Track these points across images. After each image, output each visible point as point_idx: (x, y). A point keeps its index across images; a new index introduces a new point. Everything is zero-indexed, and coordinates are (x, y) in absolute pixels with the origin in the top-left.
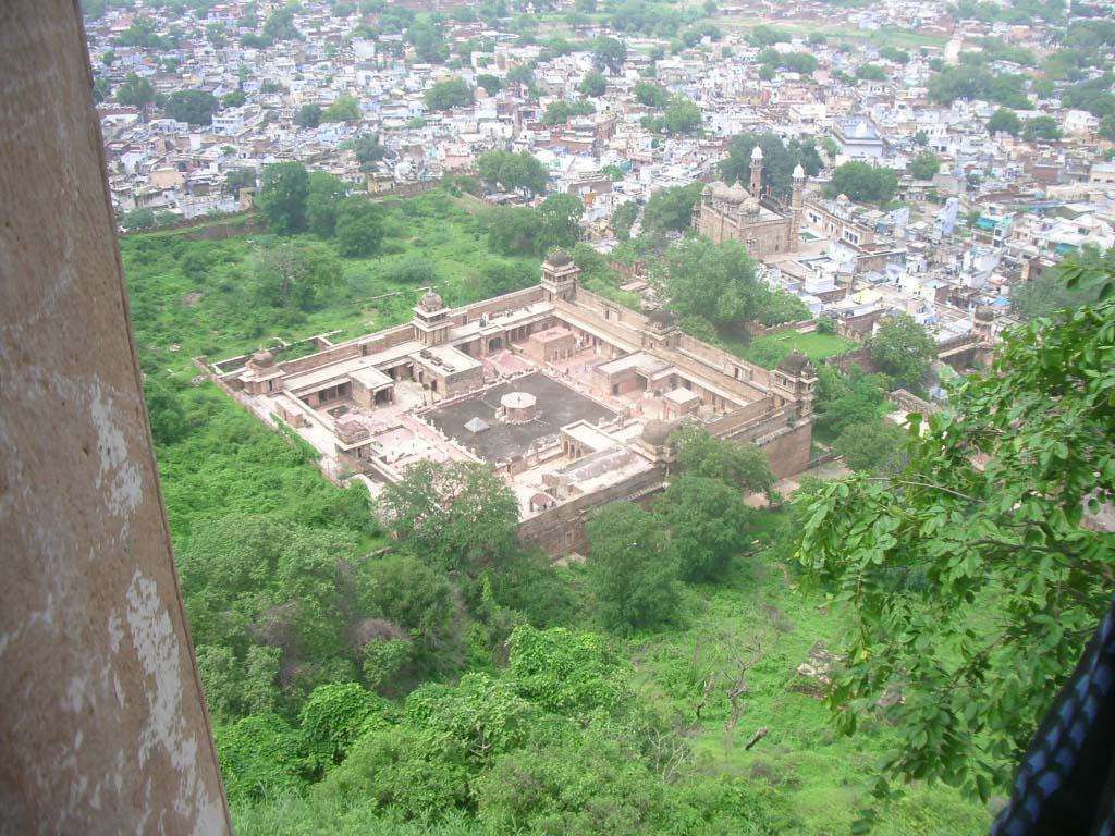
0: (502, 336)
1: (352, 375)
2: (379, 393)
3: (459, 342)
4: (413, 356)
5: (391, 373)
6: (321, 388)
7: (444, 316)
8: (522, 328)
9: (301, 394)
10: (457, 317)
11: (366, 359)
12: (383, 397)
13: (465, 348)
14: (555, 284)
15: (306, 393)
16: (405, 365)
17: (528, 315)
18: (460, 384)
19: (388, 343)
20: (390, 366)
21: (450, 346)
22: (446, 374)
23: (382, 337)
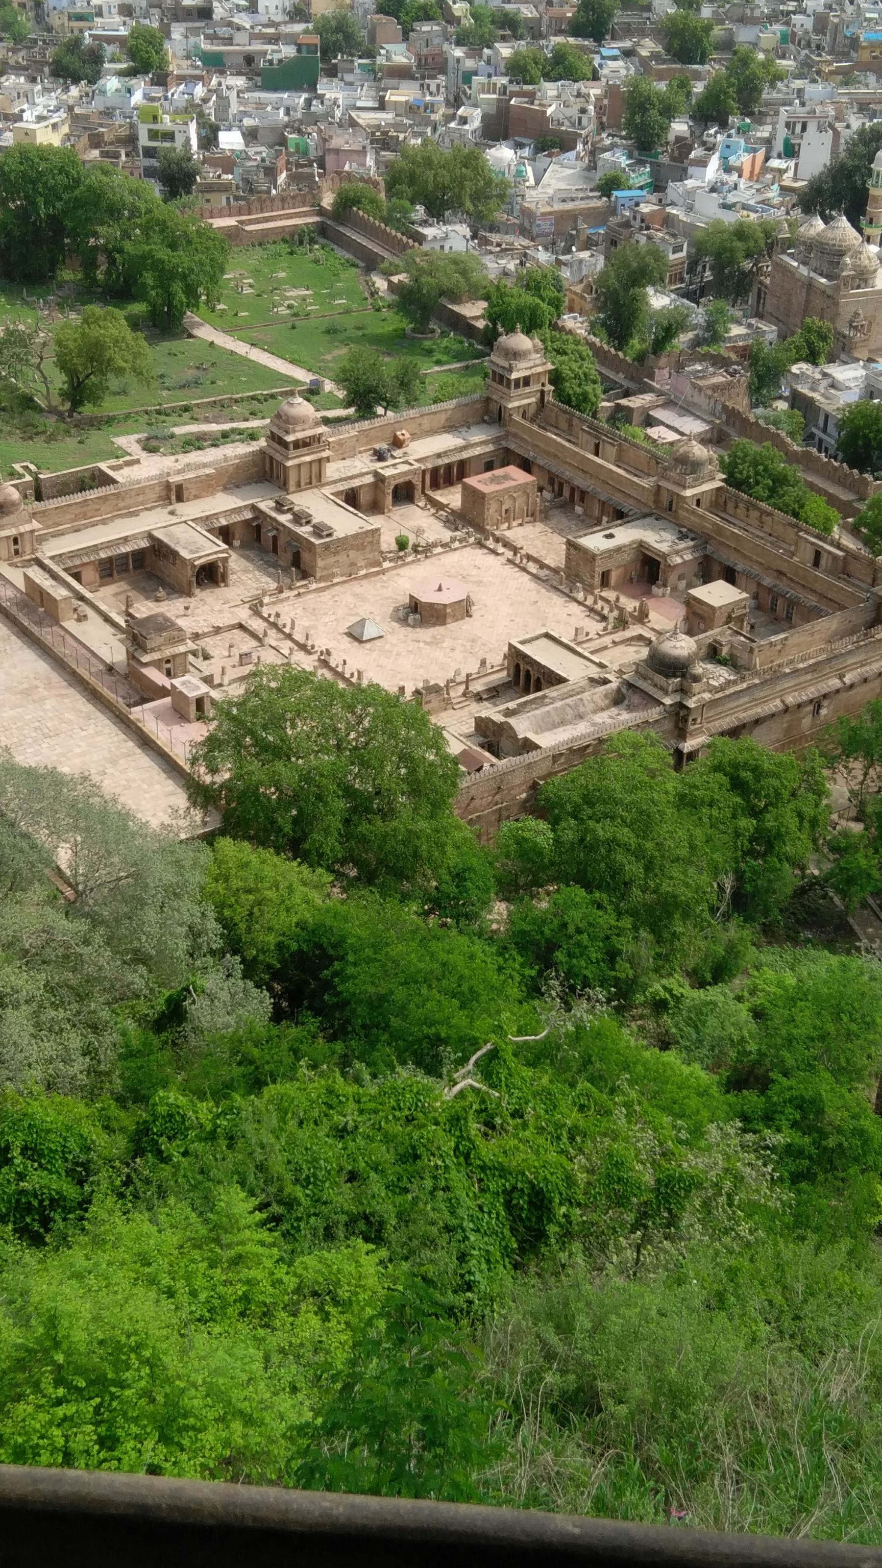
0: (417, 481)
2: (203, 568)
3: (341, 487)
5: (225, 534)
7: (317, 439)
8: (449, 467)
11: (179, 507)
13: (351, 498)
15: (77, 562)
16: (247, 523)
18: (342, 558)
20: (224, 522)
21: (327, 491)
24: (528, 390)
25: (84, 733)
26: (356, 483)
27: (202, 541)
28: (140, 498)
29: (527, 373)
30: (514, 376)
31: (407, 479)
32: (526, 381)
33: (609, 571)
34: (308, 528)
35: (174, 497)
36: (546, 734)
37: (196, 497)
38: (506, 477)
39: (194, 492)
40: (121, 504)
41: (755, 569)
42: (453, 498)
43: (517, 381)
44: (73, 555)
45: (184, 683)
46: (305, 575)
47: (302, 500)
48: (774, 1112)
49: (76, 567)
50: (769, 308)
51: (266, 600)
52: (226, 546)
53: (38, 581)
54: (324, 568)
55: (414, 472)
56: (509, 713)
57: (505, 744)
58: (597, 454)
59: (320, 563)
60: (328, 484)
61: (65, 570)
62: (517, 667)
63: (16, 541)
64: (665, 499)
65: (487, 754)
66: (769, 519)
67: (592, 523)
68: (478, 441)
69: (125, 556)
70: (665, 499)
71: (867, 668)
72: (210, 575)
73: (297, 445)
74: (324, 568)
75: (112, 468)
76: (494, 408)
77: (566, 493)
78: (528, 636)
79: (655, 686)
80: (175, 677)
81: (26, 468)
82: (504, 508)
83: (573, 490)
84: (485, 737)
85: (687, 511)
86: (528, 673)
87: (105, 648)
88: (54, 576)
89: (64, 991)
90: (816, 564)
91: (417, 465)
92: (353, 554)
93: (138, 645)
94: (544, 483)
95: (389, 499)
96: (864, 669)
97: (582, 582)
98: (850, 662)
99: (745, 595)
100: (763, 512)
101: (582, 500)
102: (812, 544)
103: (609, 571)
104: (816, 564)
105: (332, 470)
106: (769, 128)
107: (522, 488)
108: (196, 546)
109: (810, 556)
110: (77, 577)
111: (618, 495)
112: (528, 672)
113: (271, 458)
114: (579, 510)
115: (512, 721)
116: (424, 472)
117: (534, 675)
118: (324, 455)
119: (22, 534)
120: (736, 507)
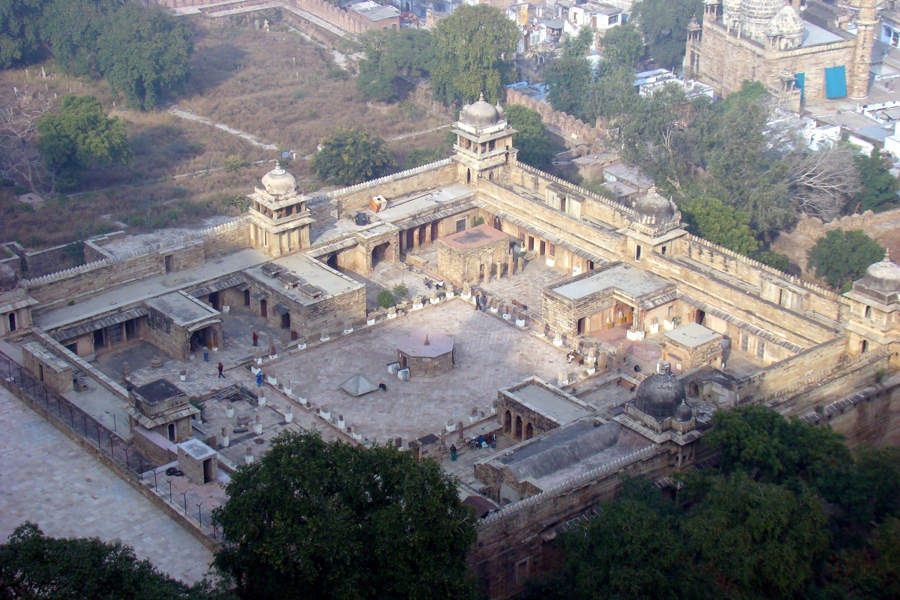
2: (196, 334)
4: (250, 272)
5: (214, 299)
11: (173, 277)
12: (200, 339)
14: (478, 155)
22: (307, 302)
25: (96, 502)
28: (132, 271)
36: (545, 478)
39: (183, 263)
40: (114, 277)
41: (725, 310)
44: (70, 328)
45: (191, 447)
48: (536, 317)
49: (72, 339)
50: (703, 68)
53: (37, 355)
56: (507, 460)
61: (62, 342)
62: (508, 412)
63: (12, 317)
66: (733, 262)
78: (516, 384)
79: (645, 425)
80: (181, 440)
81: (13, 247)
83: (543, 245)
84: (485, 483)
86: (518, 418)
87: (107, 417)
88: (53, 351)
93: (142, 411)
100: (726, 257)
101: (553, 253)
110: (73, 348)
111: (459, 210)
113: (256, 226)
115: (512, 466)
119: (18, 310)
120: (701, 253)
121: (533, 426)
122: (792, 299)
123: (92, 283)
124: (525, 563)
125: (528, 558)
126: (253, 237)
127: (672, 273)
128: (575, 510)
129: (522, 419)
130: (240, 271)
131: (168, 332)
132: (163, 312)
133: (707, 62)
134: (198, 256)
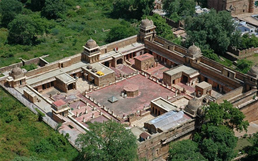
1: (57, 77)
2: (69, 85)
3: (104, 61)
5: (74, 75)
6: (43, 83)
7: (97, 50)
9: (34, 86)
10: (102, 50)
13: (106, 64)
15: (36, 85)
17: (133, 48)
19: (69, 63)
21: (100, 62)
23: (69, 59)
24: (150, 33)
26: (108, 60)
27: (68, 78)
29: (149, 29)
30: (146, 30)
31: (120, 58)
32: (149, 31)
33: (175, 80)
34: (91, 70)
35: (61, 67)
37: (66, 66)
38: (146, 56)
39: (66, 65)
42: (132, 61)
43: (147, 31)
46: (225, 93)
47: (93, 65)
51: (86, 93)
52: (75, 79)
54: (101, 83)
55: (122, 56)
57: (152, 130)
58: (169, 49)
59: (100, 82)
60: (100, 61)
62: (153, 107)
64: (188, 60)
65: (148, 133)
67: (169, 67)
68: (139, 46)
69: (49, 83)
70: (188, 60)
71: (244, 103)
72: (72, 86)
73: (92, 51)
74: (101, 83)
75: (154, 101)
76: (141, 38)
77: (162, 59)
82: (146, 64)
85: (194, 63)
86: (156, 110)
89: (105, 100)
90: (228, 76)
91: (123, 54)
92: (108, 79)
94: (156, 57)
95: (116, 63)
96: (243, 104)
97: (168, 84)
98: (240, 102)
99: (211, 85)
102: (227, 70)
103: (175, 80)
104: (228, 76)
105: (101, 57)
106: (100, 105)
107: (150, 59)
108: (67, 80)
109: (227, 74)
112: (156, 109)
113: (85, 55)
114: (165, 63)
116: (125, 56)
117: (158, 110)
118: (99, 53)
121: (160, 111)
122: (231, 75)
123: (41, 71)
124: (158, 150)
125: (158, 149)
126: (84, 58)
127: (198, 67)
128: (171, 136)
129: (157, 109)
130: (81, 68)
131: (62, 85)
132: (60, 79)
133: (210, 3)
134: (70, 63)
